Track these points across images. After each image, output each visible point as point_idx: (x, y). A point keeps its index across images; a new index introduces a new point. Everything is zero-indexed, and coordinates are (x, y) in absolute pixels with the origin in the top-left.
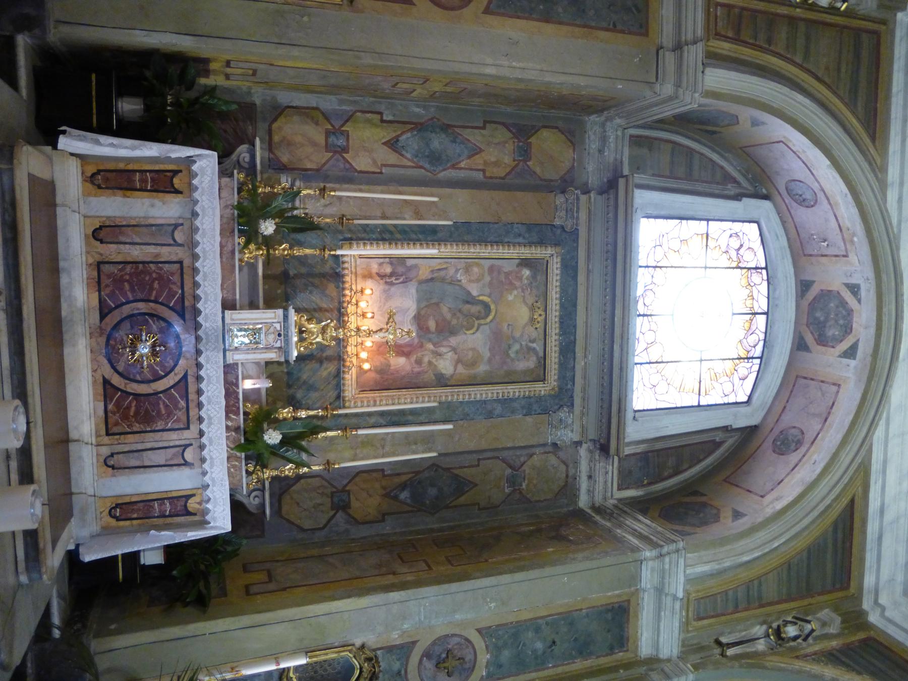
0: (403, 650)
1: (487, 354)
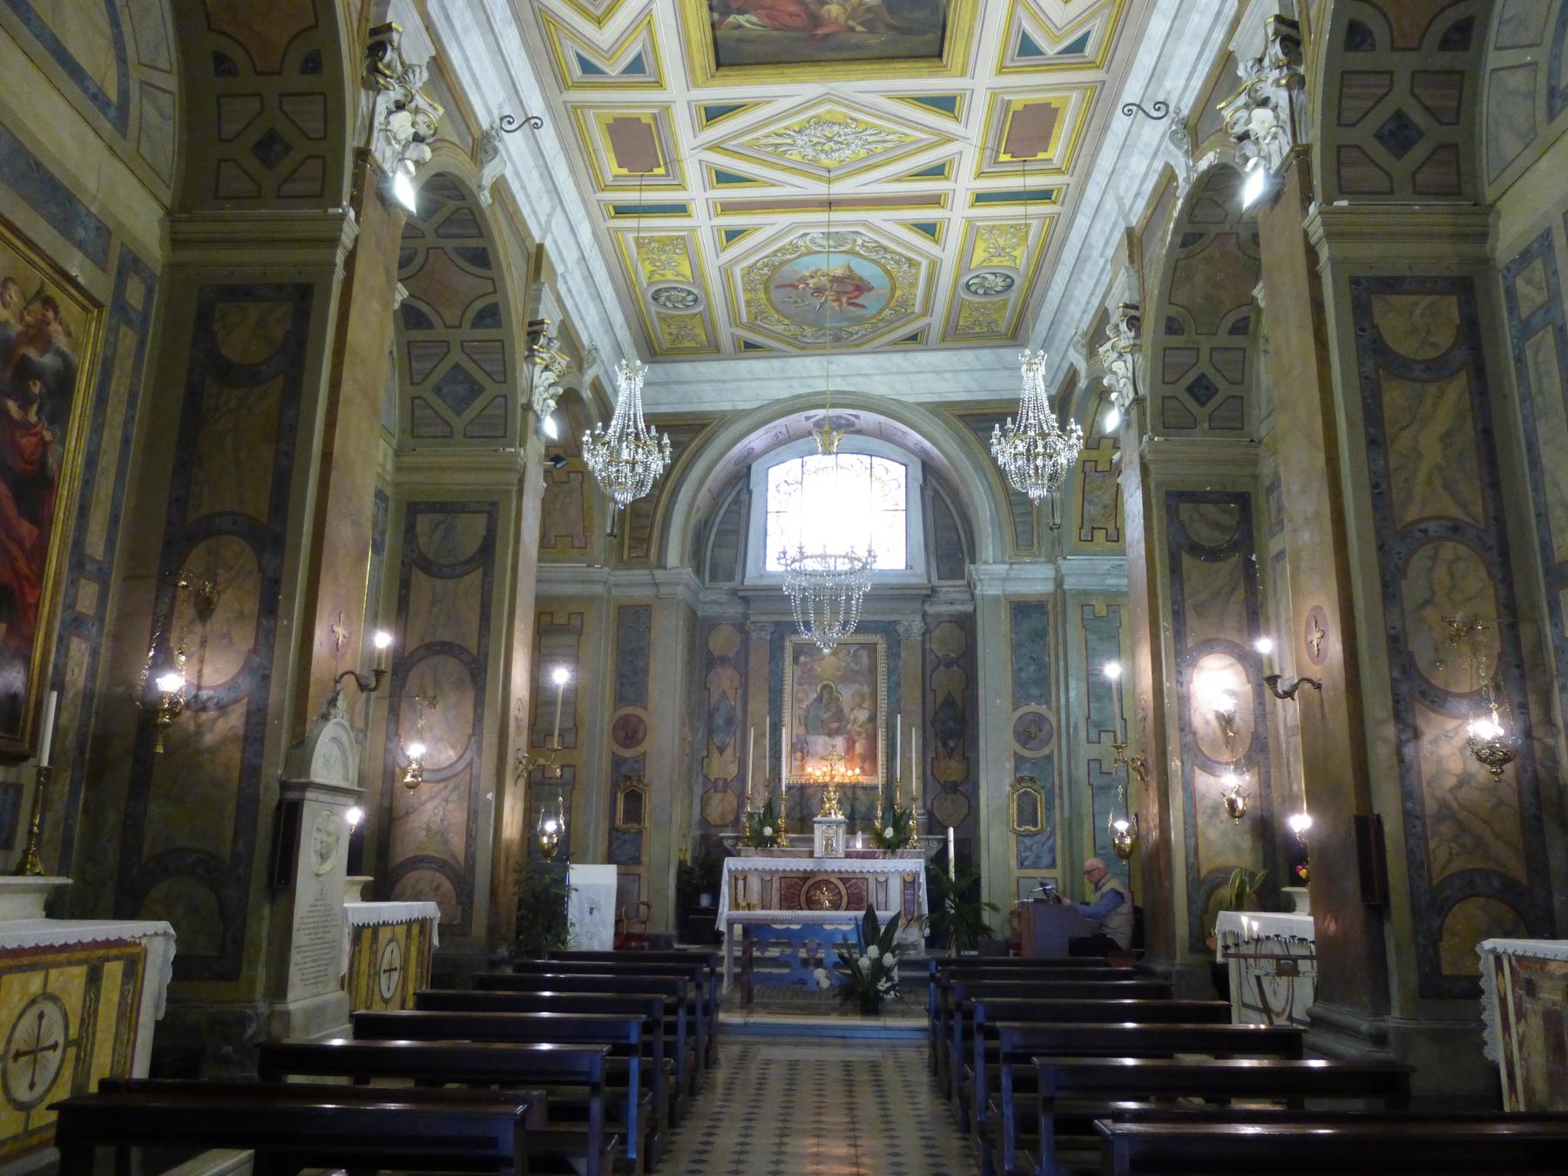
0: (1019, 760)
1: (857, 686)
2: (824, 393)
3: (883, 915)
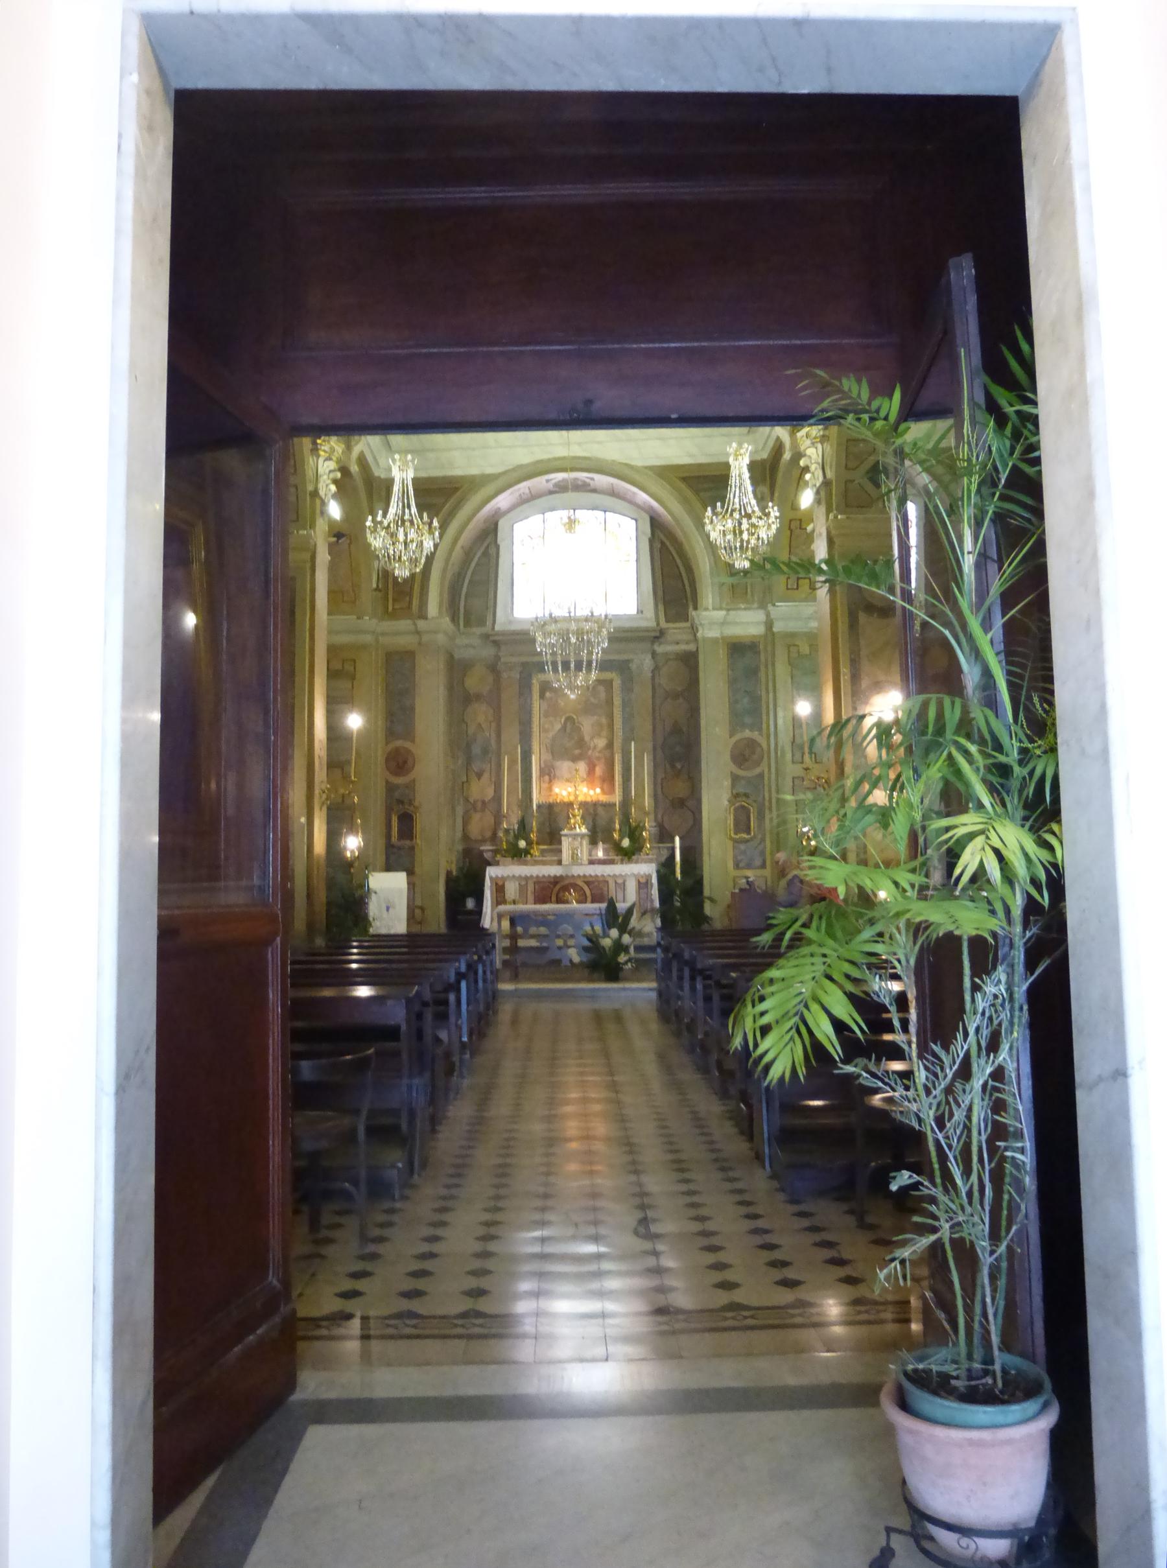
0: (735, 779)
2: (564, 458)
3: (622, 906)
